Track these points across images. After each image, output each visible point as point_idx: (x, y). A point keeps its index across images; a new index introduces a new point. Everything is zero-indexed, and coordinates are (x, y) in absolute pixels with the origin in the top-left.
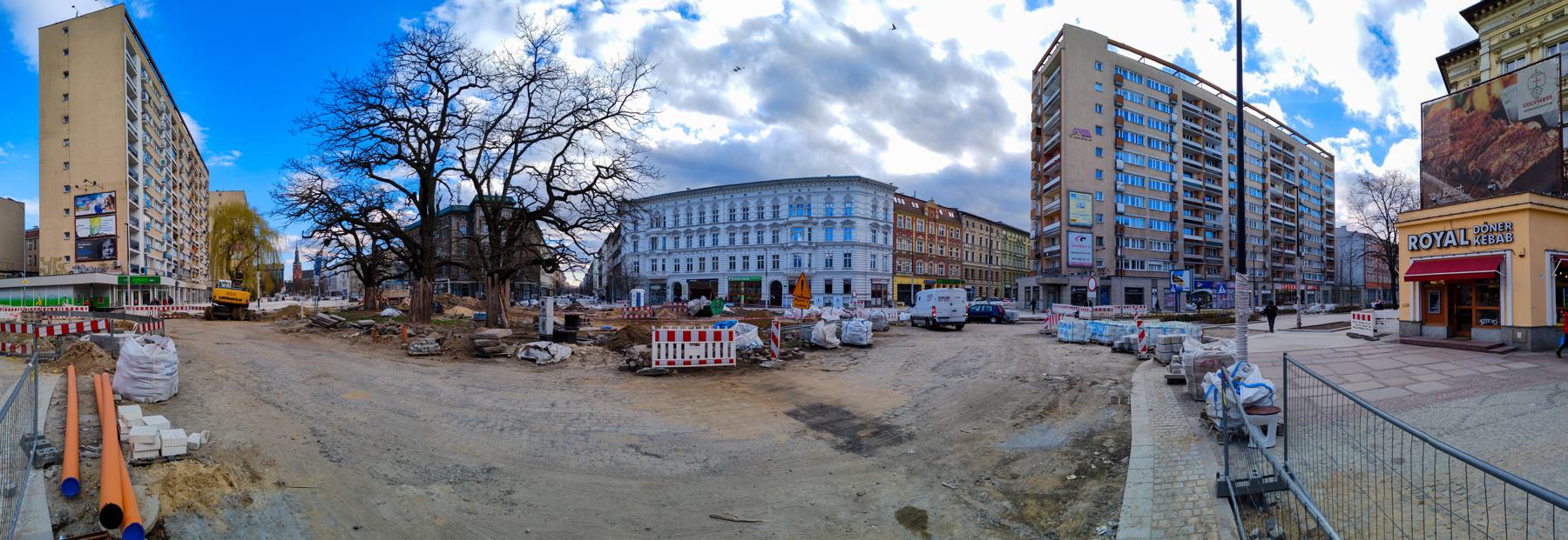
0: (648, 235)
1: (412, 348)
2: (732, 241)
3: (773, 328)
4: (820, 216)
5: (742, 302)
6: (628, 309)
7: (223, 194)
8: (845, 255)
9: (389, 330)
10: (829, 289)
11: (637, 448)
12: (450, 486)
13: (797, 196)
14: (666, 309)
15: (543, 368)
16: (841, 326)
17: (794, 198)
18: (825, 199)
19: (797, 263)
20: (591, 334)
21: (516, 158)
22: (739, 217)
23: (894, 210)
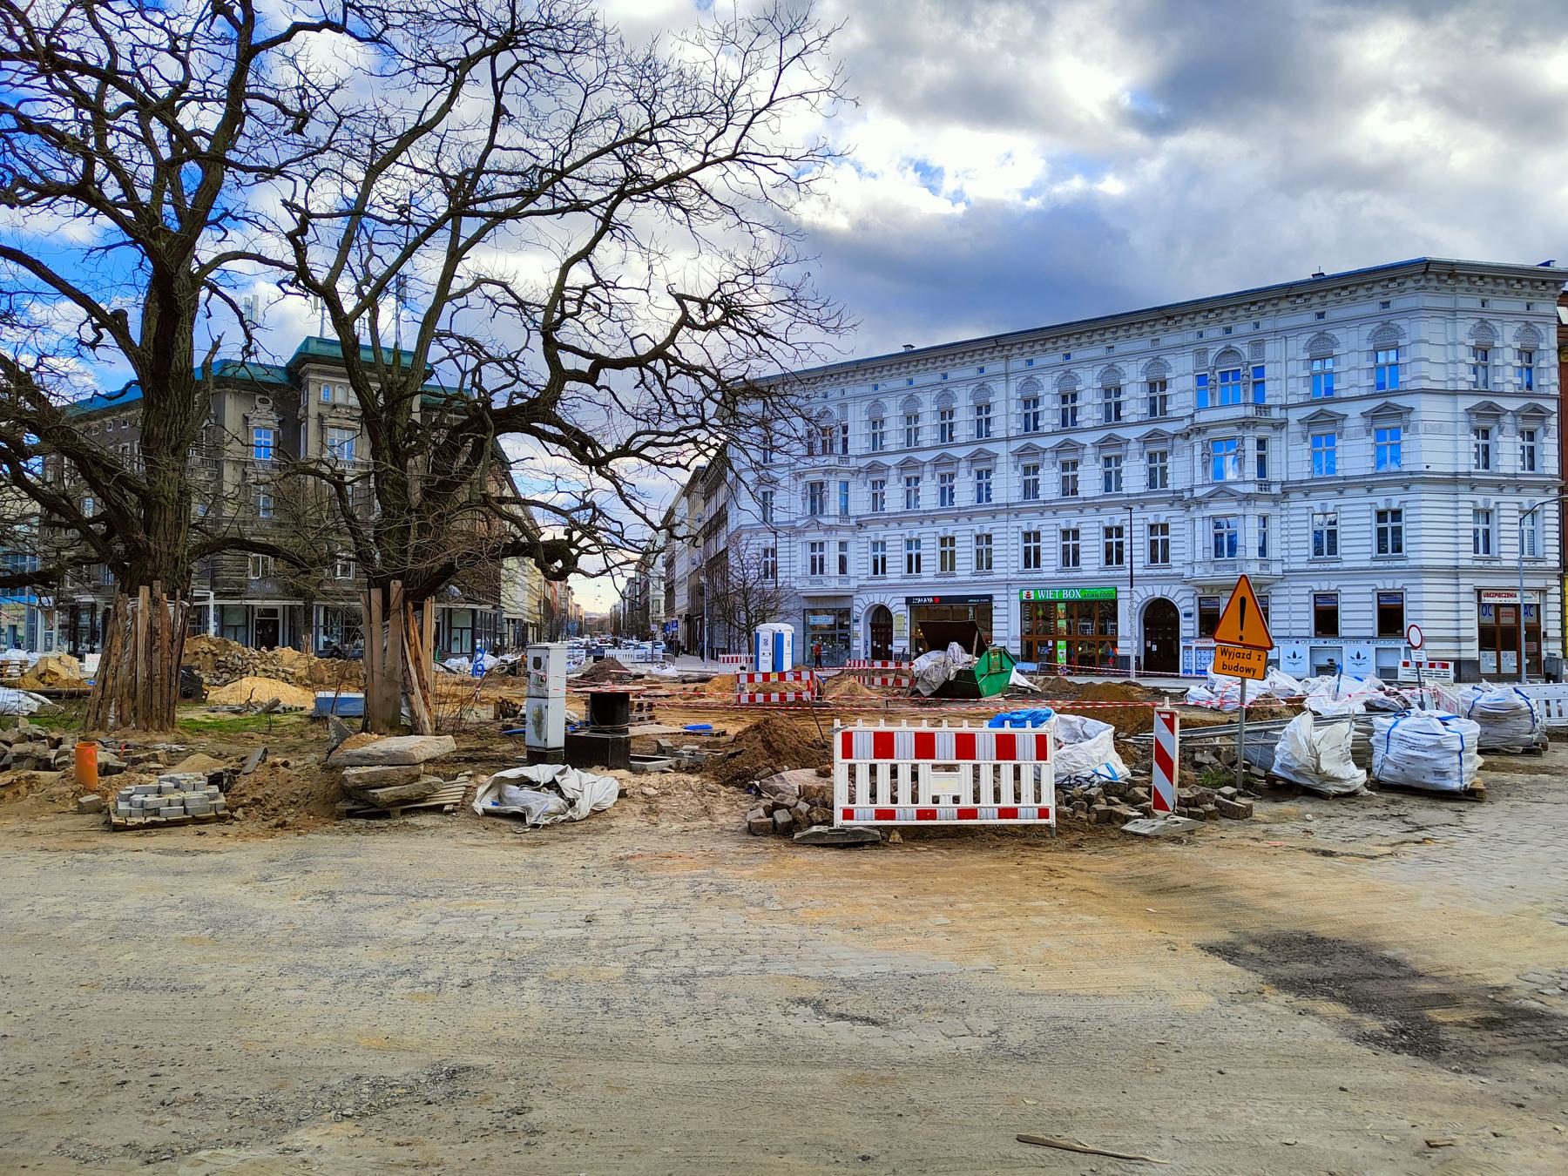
1: (122, 806)
2: (1031, 489)
3: (1160, 731)
4: (1293, 400)
5: (1062, 659)
6: (751, 678)
8: (1381, 516)
9: (20, 758)
10: (1326, 621)
11: (818, 1006)
12: (347, 1124)
13: (1220, 347)
14: (852, 680)
15: (545, 834)
16: (1370, 733)
17: (1211, 355)
18: (1310, 346)
19: (1225, 545)
20: (665, 743)
21: (455, 256)
22: (1049, 418)
23: (1559, 351)
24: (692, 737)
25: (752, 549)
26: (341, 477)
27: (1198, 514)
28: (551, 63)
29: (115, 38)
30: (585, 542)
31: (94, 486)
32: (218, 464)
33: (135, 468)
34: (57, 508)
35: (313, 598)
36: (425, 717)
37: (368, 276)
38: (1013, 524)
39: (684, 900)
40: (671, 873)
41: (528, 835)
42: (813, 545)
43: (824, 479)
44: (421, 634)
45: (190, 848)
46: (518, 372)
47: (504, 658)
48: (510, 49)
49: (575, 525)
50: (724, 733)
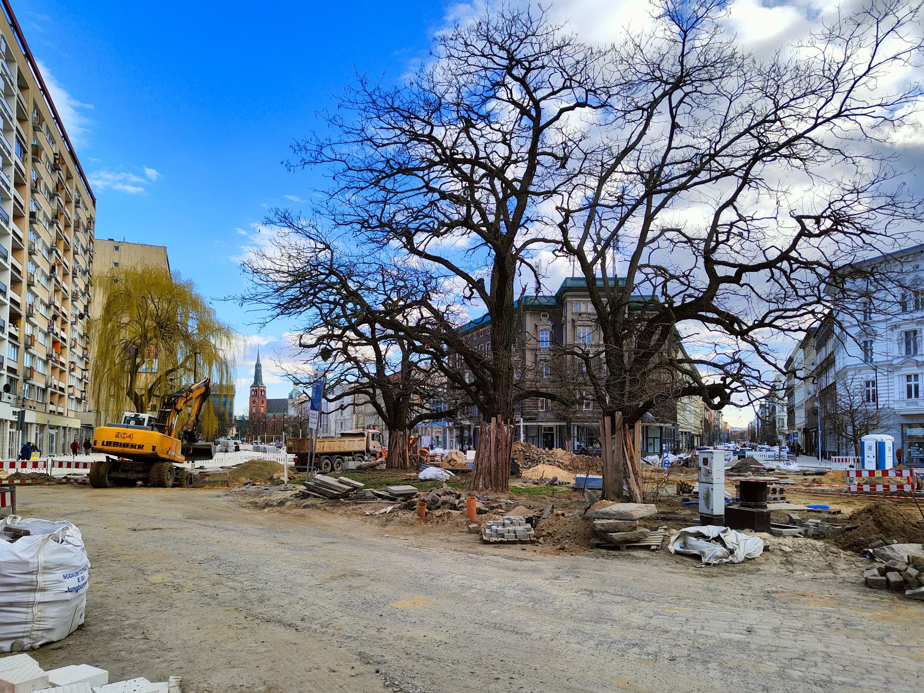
1: (488, 531)
6: (859, 474)
7: (121, 248)
9: (444, 503)
15: (715, 570)
20: (795, 517)
21: (649, 218)
24: (814, 514)
25: (856, 382)
26: (588, 355)
28: (708, 88)
29: (478, 142)
30: (735, 385)
31: (471, 368)
32: (523, 351)
33: (489, 357)
34: (455, 378)
35: (571, 420)
36: (637, 492)
37: (600, 239)
39: (817, 627)
40: (806, 607)
41: (703, 569)
43: (917, 328)
44: (633, 443)
45: (519, 557)
46: (689, 282)
47: (680, 456)
48: (680, 87)
49: (727, 374)
50: (839, 512)
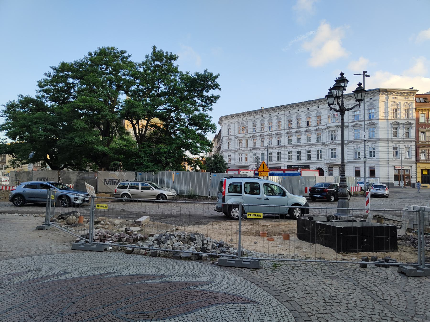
0: (236, 138)
4: (350, 121)
27: (327, 148)
38: (286, 150)
42: (239, 154)
